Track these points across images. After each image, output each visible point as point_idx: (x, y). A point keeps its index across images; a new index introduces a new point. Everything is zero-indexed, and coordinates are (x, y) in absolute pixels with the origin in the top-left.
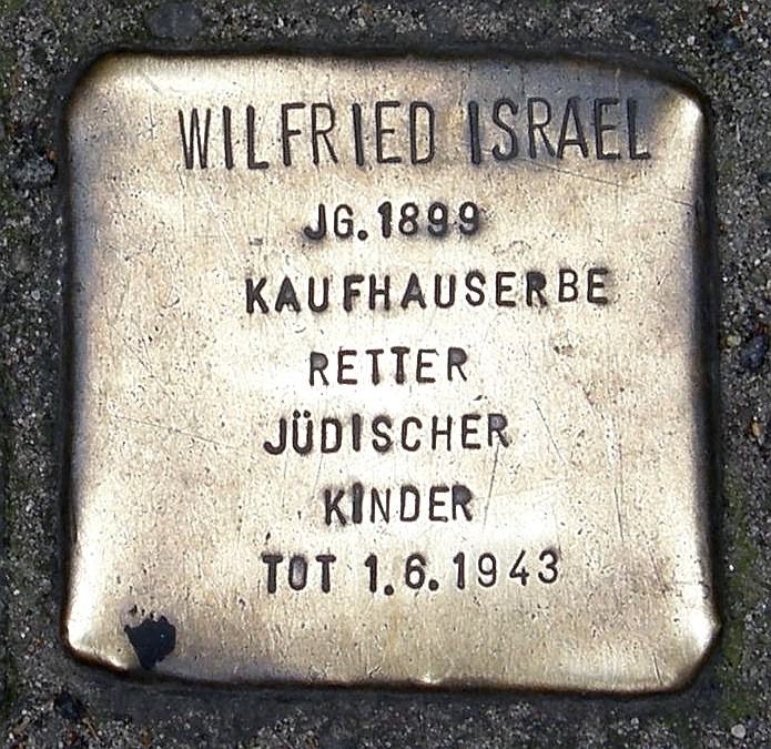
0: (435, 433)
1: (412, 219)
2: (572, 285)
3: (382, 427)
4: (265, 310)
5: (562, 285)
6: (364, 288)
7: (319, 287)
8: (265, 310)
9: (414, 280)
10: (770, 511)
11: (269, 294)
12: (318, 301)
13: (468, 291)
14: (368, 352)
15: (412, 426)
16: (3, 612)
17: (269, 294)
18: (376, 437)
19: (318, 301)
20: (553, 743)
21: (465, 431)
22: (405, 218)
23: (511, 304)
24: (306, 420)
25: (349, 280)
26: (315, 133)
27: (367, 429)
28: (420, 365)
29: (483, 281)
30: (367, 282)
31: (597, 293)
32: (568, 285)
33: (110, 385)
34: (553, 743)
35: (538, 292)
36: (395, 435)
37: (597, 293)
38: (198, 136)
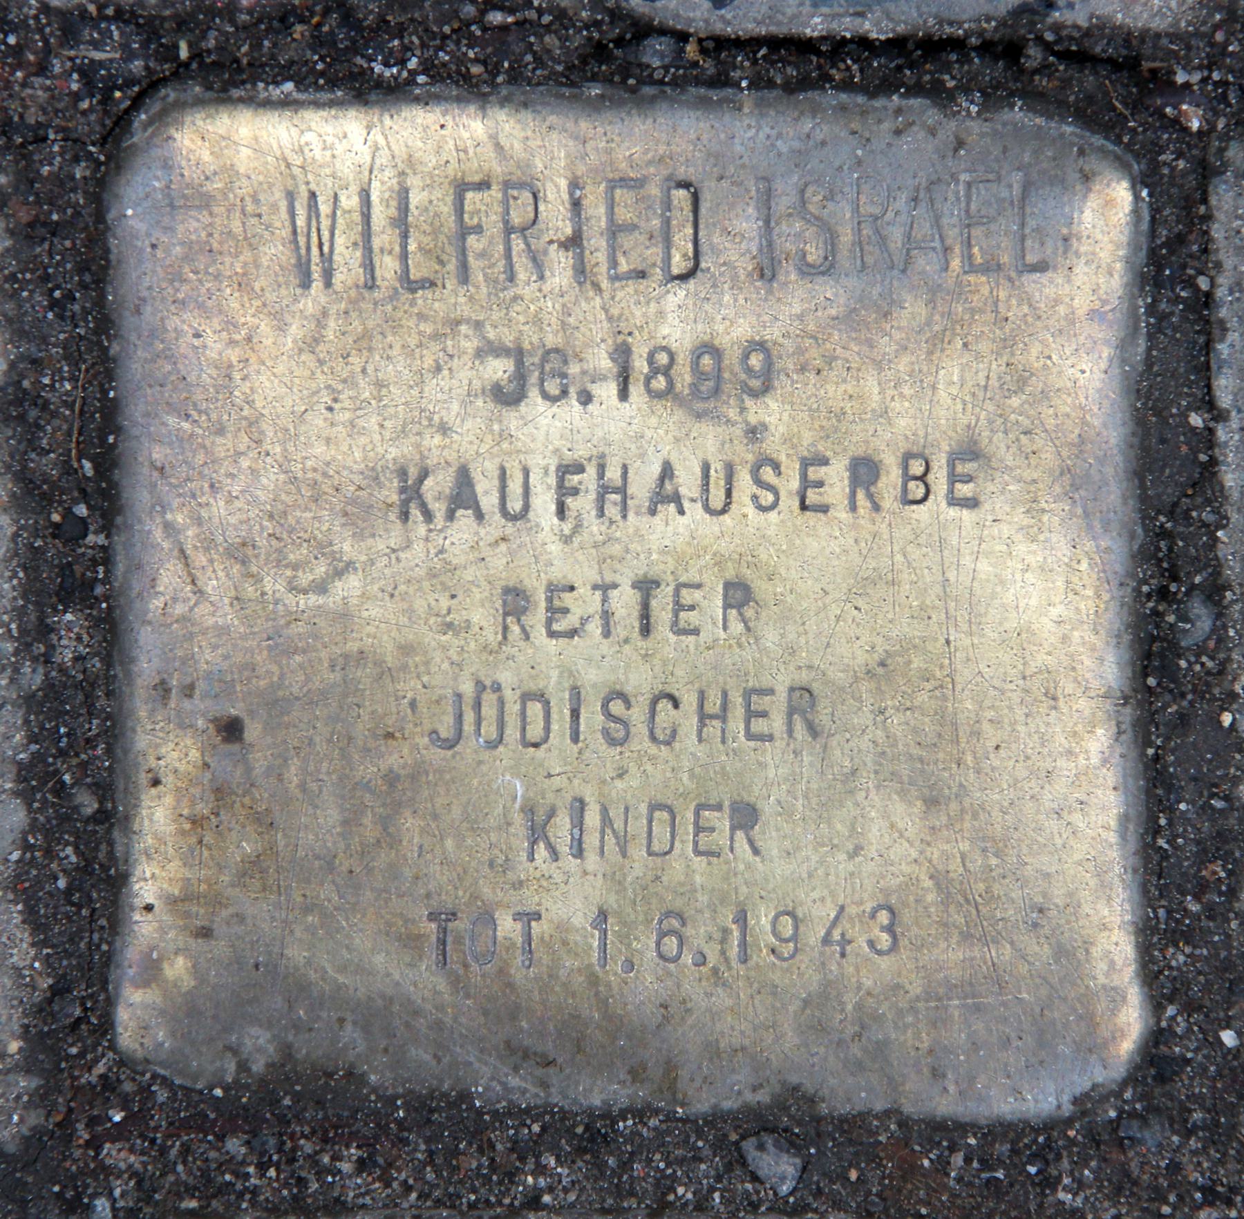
0: (703, 717)
1: (666, 371)
2: (922, 478)
3: (617, 707)
4: (428, 516)
5: (907, 477)
6: (589, 478)
7: (515, 487)
8: (428, 516)
9: (667, 472)
10: (132, 1213)
11: (436, 487)
12: (515, 505)
13: (755, 489)
14: (595, 587)
15: (664, 705)
16: (558, 1213)
17: (436, 487)
18: (759, 492)
19: (515, 505)
20: (701, 1204)
21: (751, 714)
22: (655, 370)
23: (824, 509)
24: (494, 697)
25: (566, 470)
26: (508, 230)
27: (592, 717)
28: (679, 607)
29: (628, 704)
30: (591, 471)
31: (964, 490)
32: (916, 478)
33: (31, 225)
34: (701, 1204)
35: (868, 490)
36: (637, 716)
37: (964, 490)
38: (319, 230)
